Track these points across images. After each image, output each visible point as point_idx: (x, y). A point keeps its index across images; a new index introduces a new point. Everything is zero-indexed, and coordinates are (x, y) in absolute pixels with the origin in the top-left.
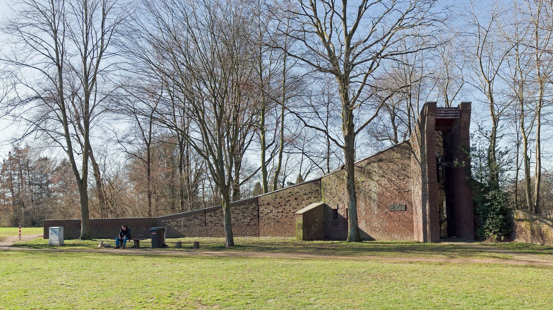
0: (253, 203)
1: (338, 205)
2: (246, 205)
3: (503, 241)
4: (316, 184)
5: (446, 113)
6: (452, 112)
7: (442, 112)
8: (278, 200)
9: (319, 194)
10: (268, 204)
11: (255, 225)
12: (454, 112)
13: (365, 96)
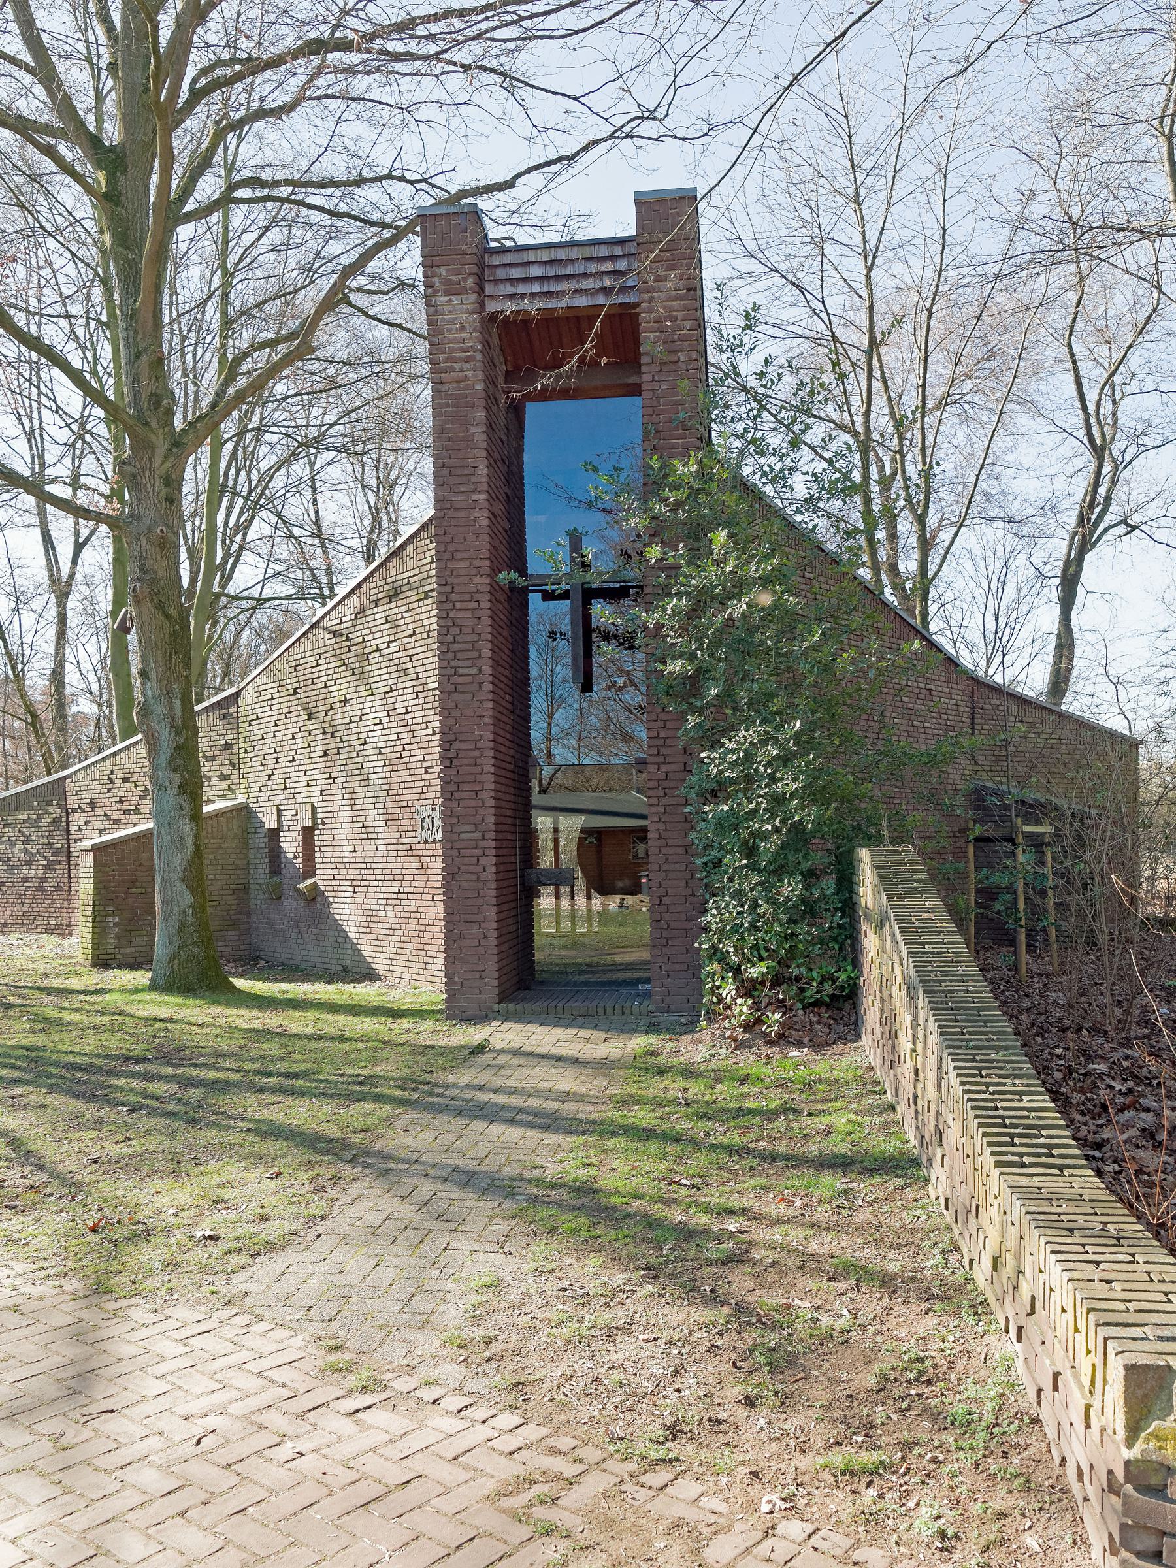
0: (49, 803)
1: (279, 811)
2: (31, 807)
3: (781, 1039)
4: (225, 717)
5: (557, 278)
6: (593, 267)
7: (536, 271)
8: (119, 789)
9: (232, 764)
10: (92, 805)
11: (58, 888)
12: (608, 266)
13: (946, 371)
